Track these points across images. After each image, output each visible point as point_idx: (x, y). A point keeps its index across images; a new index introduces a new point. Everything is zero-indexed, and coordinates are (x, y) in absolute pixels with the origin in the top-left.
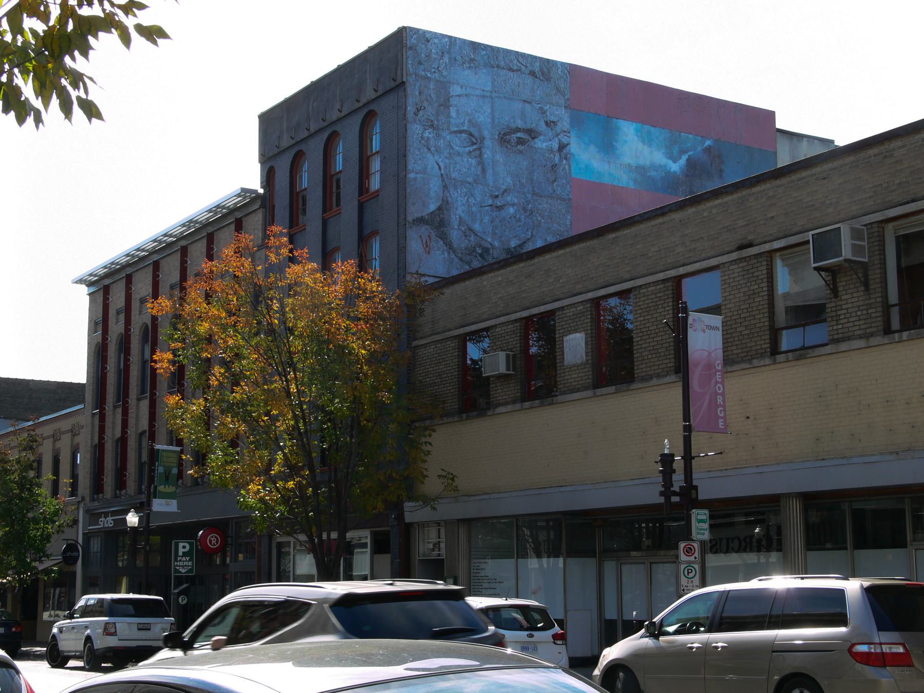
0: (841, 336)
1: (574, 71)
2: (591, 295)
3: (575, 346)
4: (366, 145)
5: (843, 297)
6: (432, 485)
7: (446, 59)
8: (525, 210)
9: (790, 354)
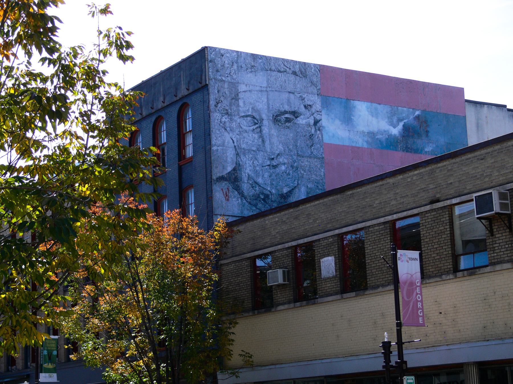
0: (496, 260)
1: (323, 69)
2: (337, 232)
3: (328, 265)
4: (183, 126)
5: (497, 236)
6: (236, 360)
7: (235, 67)
8: (292, 167)
9: (465, 272)
